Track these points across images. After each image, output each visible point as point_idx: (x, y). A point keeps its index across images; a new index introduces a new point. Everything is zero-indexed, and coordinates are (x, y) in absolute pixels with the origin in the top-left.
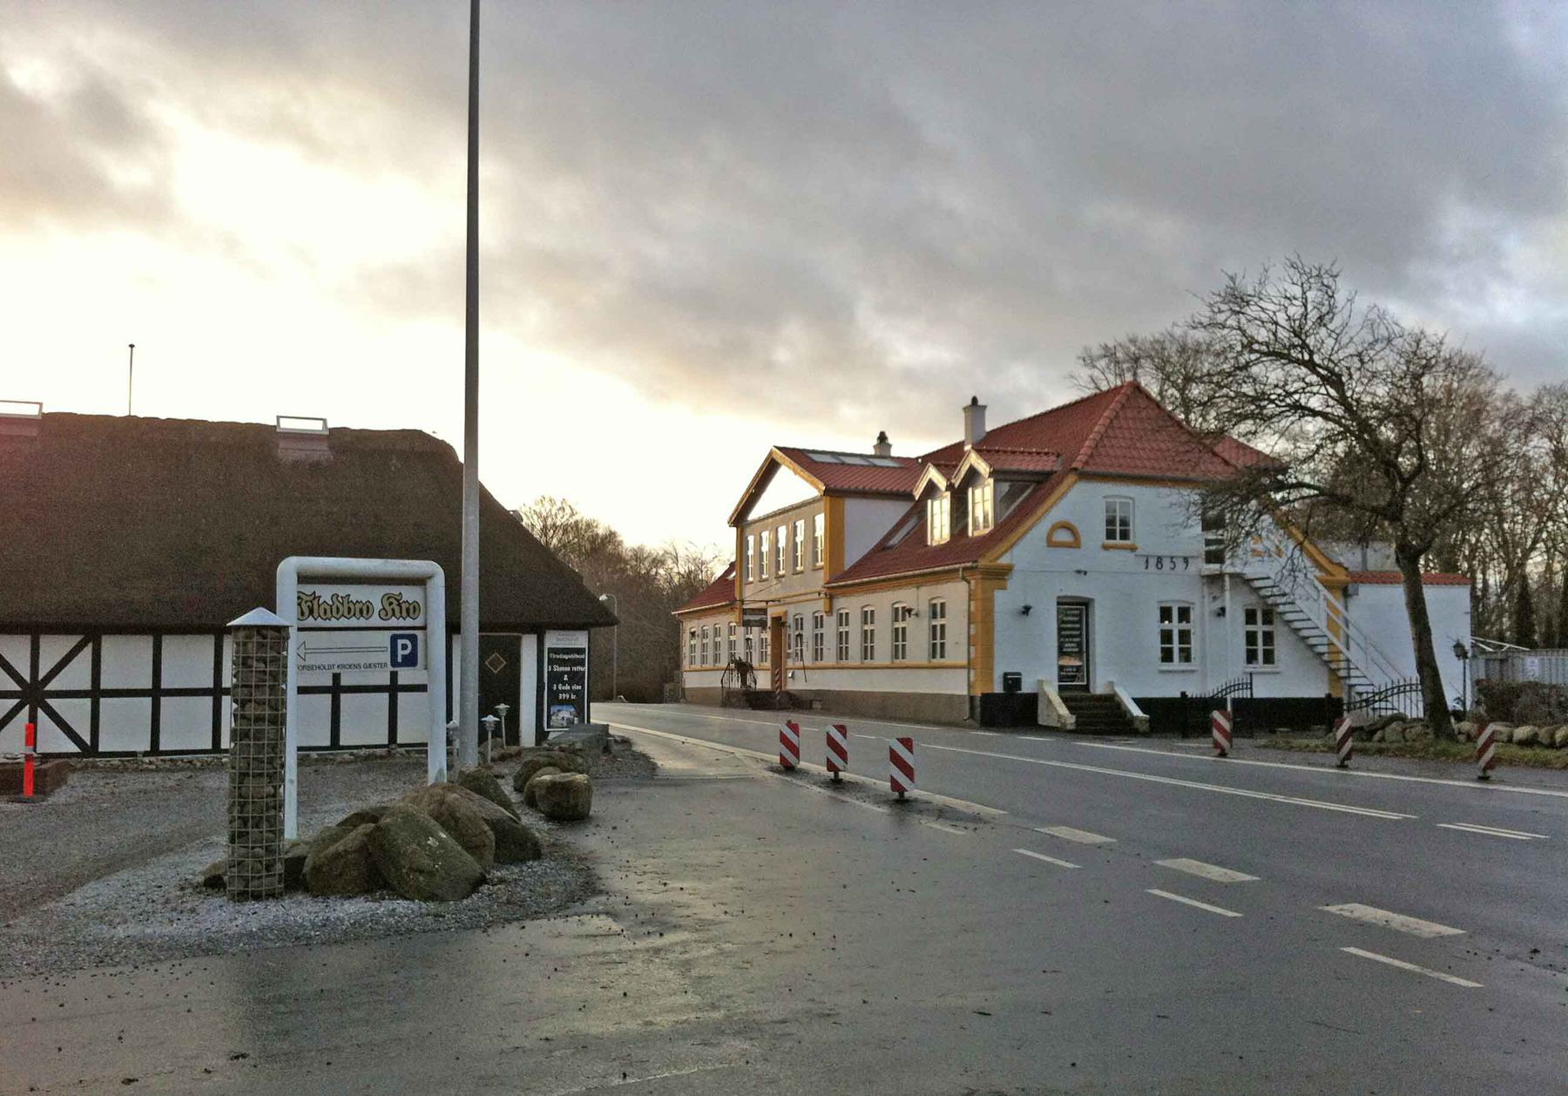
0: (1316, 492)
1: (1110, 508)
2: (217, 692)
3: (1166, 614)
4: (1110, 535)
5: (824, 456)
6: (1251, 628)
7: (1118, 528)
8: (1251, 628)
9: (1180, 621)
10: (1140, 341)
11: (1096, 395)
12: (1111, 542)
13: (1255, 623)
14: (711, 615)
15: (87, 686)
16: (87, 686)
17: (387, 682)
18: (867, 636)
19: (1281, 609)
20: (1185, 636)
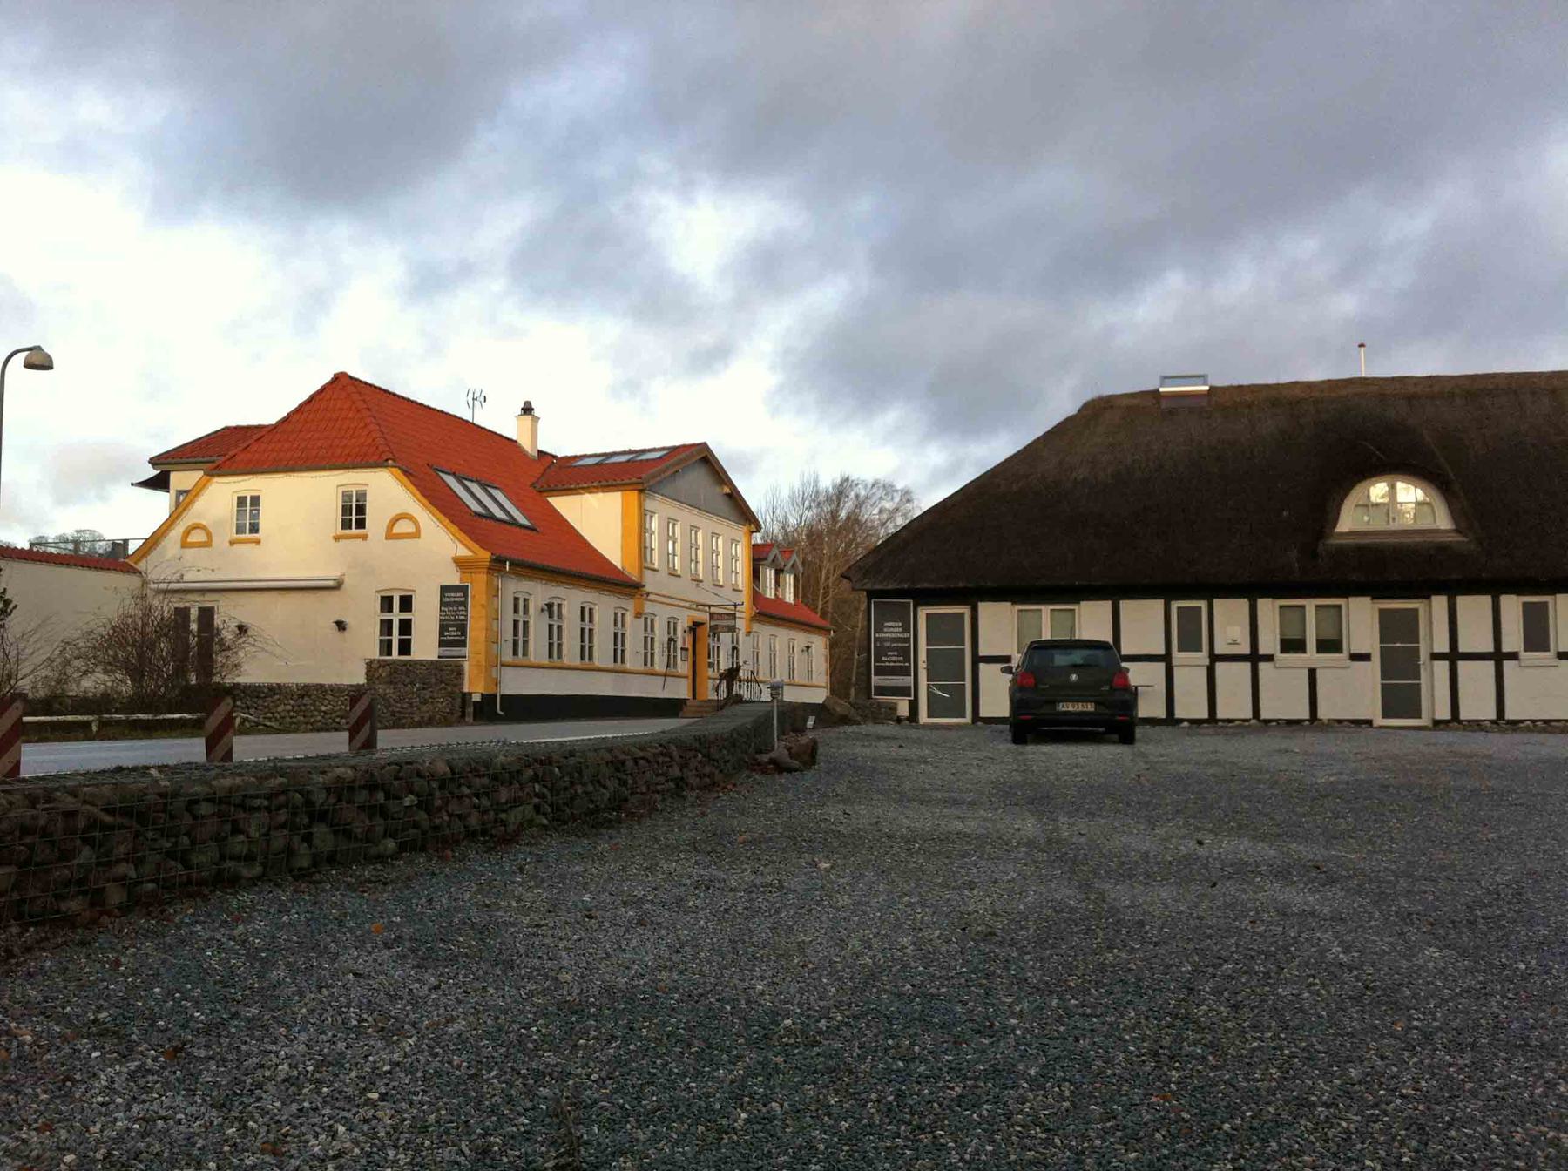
0: (466, 482)
1: (347, 496)
2: (977, 660)
3: (387, 603)
4: (346, 524)
5: (494, 505)
6: (387, 616)
7: (354, 517)
8: (405, 616)
9: (401, 610)
10: (831, 489)
11: (467, 421)
12: (348, 532)
13: (390, 610)
14: (805, 631)
15: (1490, 665)
16: (1490, 665)
17: (1446, 664)
18: (586, 635)
19: (901, 630)
20: (406, 626)
